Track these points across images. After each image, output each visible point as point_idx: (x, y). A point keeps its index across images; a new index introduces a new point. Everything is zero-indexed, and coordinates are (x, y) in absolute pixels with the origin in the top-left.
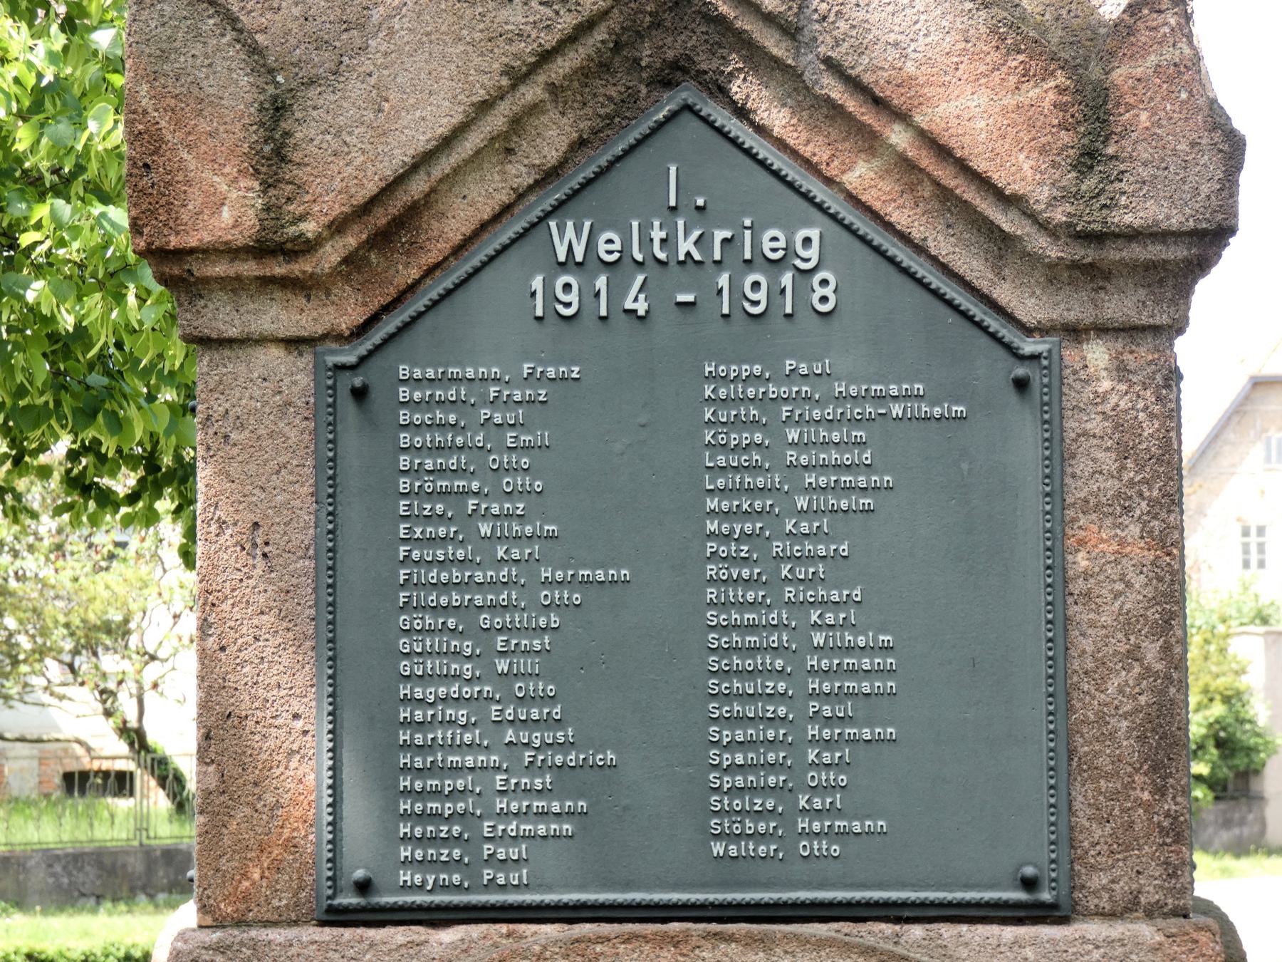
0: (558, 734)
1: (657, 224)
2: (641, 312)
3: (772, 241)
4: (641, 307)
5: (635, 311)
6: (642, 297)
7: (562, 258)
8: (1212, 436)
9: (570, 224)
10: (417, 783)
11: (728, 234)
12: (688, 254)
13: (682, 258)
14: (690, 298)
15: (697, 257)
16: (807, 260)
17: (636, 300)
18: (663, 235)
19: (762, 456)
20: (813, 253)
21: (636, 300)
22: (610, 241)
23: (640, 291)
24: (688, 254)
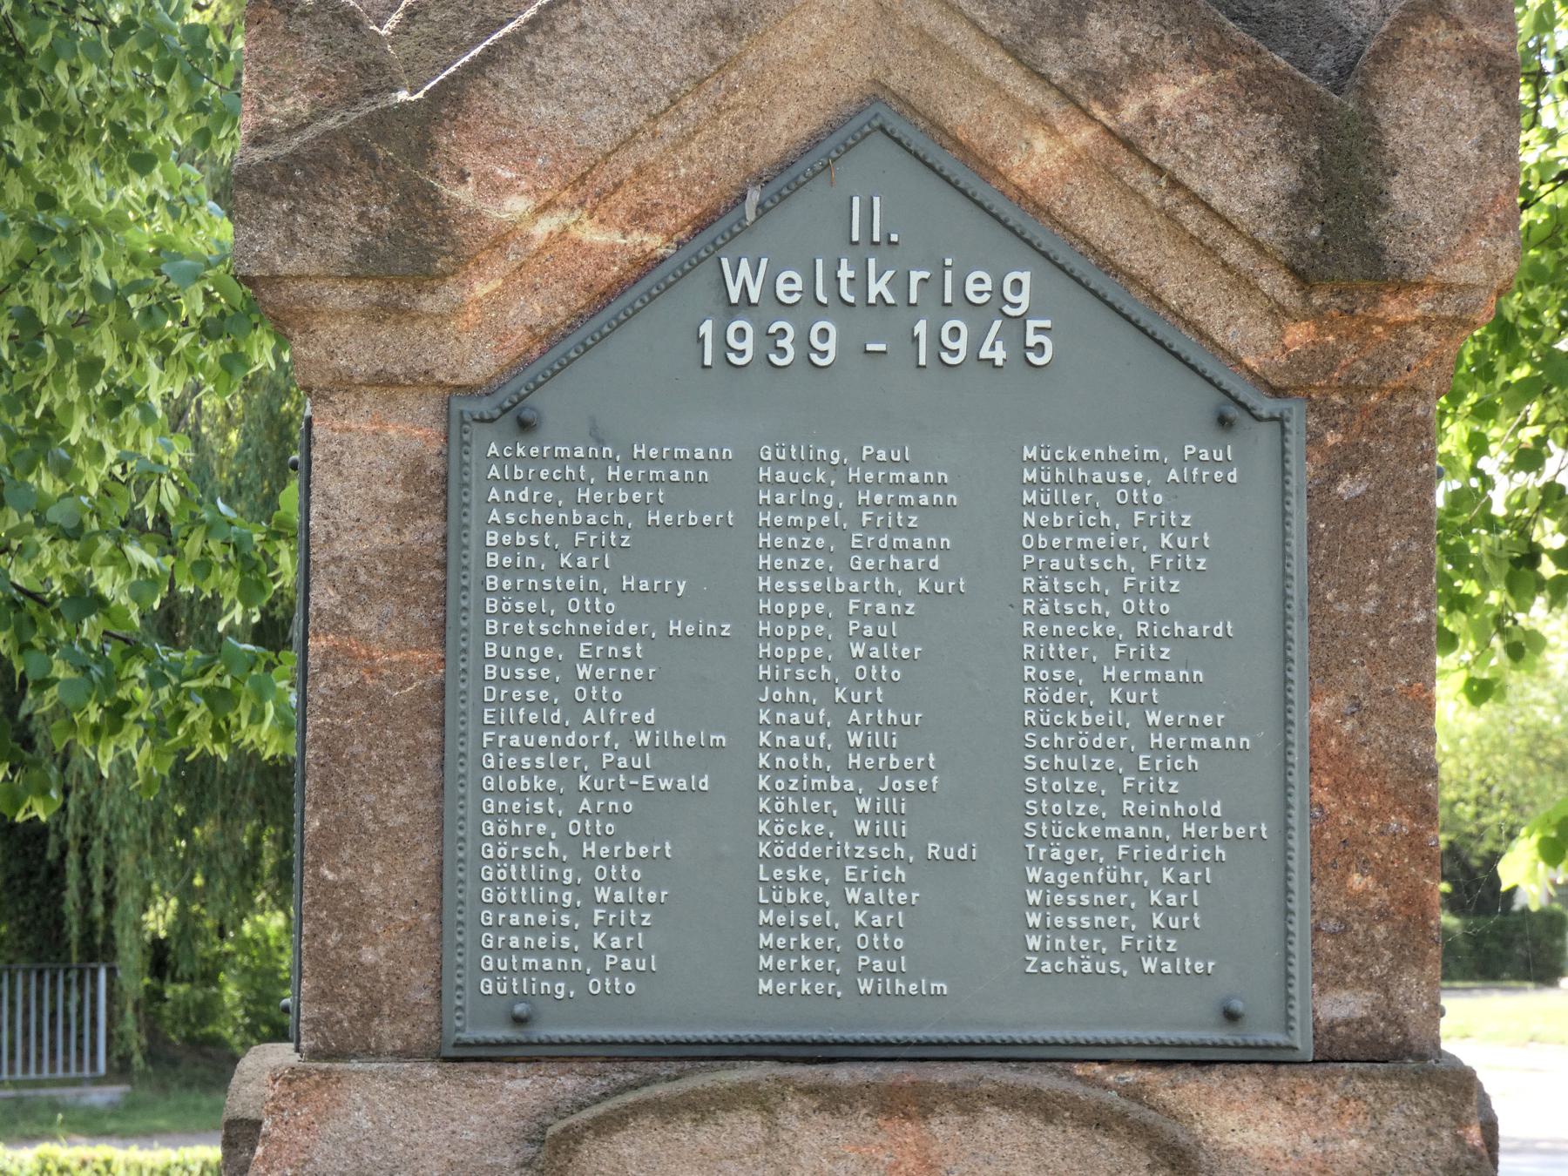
0: (1112, 964)
1: (844, 262)
2: (999, 362)
3: (978, 285)
4: (999, 356)
5: (993, 360)
6: (999, 344)
7: (734, 299)
8: (1453, 993)
9: (744, 263)
10: (641, 849)
11: (926, 275)
12: (880, 295)
13: (872, 300)
14: (882, 347)
15: (890, 299)
16: (1017, 305)
17: (993, 347)
18: (851, 274)
19: (1103, 605)
20: (1024, 299)
21: (993, 347)
22: (980, 281)
23: (996, 338)
24: (880, 295)
